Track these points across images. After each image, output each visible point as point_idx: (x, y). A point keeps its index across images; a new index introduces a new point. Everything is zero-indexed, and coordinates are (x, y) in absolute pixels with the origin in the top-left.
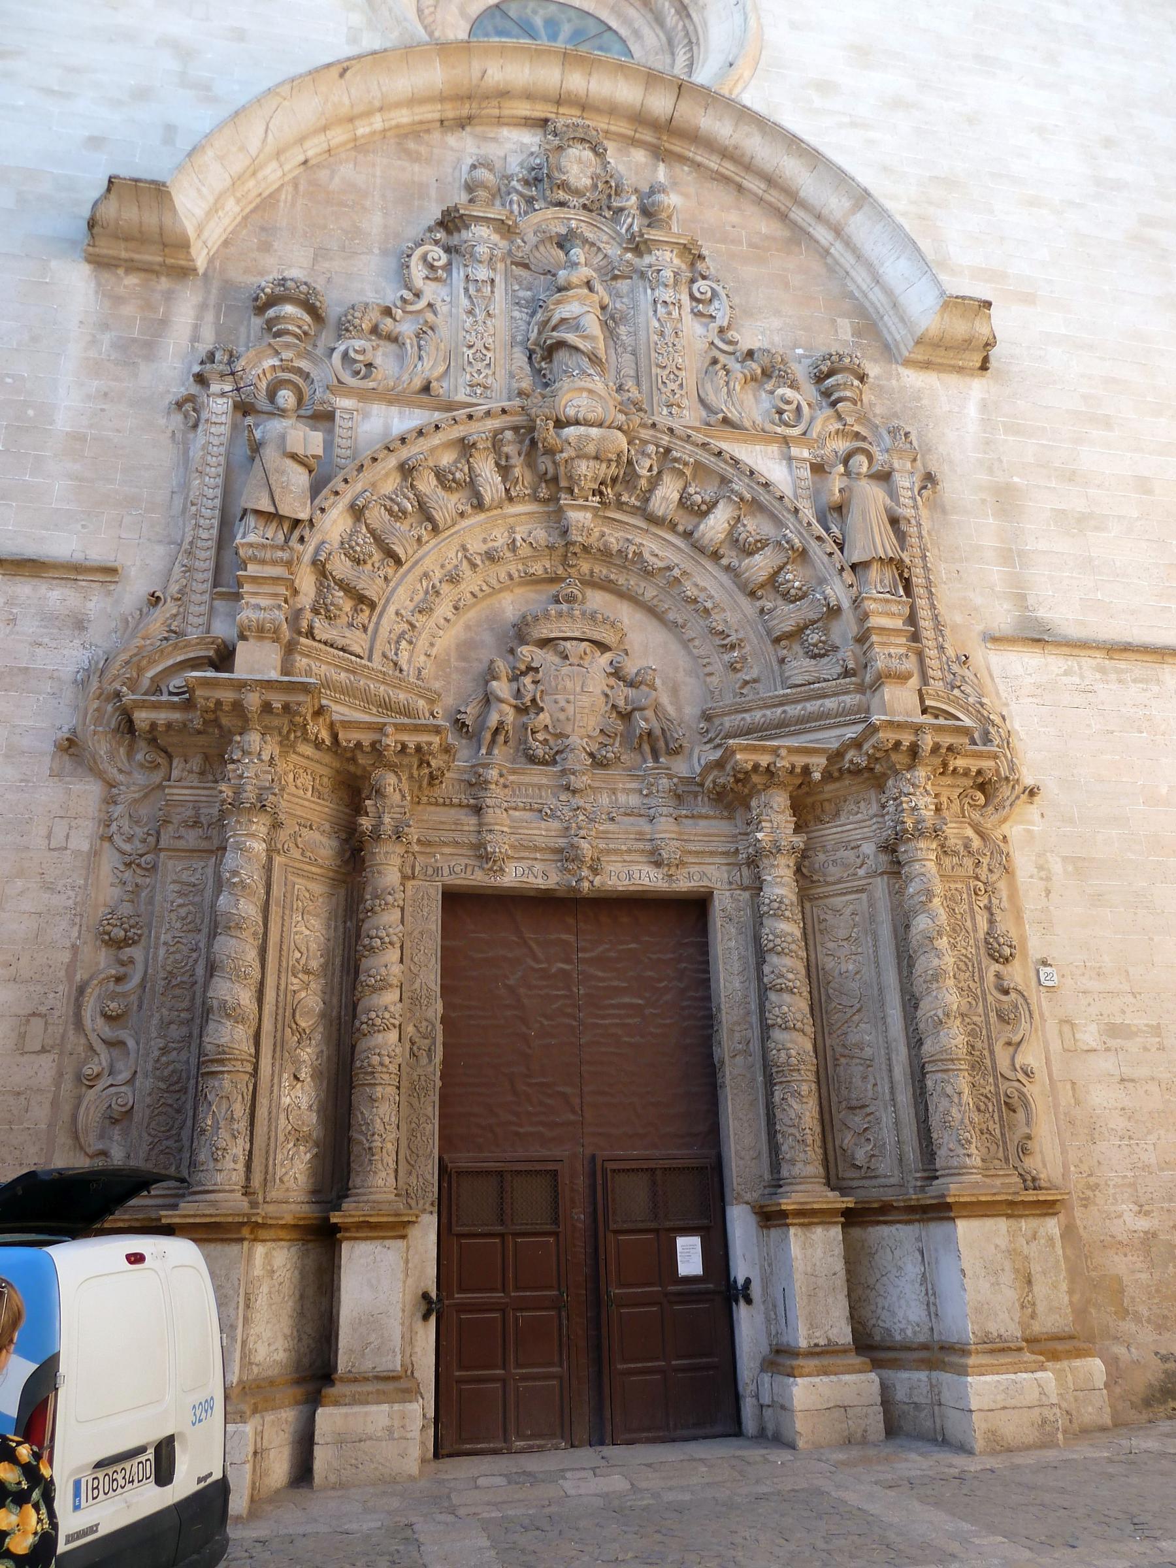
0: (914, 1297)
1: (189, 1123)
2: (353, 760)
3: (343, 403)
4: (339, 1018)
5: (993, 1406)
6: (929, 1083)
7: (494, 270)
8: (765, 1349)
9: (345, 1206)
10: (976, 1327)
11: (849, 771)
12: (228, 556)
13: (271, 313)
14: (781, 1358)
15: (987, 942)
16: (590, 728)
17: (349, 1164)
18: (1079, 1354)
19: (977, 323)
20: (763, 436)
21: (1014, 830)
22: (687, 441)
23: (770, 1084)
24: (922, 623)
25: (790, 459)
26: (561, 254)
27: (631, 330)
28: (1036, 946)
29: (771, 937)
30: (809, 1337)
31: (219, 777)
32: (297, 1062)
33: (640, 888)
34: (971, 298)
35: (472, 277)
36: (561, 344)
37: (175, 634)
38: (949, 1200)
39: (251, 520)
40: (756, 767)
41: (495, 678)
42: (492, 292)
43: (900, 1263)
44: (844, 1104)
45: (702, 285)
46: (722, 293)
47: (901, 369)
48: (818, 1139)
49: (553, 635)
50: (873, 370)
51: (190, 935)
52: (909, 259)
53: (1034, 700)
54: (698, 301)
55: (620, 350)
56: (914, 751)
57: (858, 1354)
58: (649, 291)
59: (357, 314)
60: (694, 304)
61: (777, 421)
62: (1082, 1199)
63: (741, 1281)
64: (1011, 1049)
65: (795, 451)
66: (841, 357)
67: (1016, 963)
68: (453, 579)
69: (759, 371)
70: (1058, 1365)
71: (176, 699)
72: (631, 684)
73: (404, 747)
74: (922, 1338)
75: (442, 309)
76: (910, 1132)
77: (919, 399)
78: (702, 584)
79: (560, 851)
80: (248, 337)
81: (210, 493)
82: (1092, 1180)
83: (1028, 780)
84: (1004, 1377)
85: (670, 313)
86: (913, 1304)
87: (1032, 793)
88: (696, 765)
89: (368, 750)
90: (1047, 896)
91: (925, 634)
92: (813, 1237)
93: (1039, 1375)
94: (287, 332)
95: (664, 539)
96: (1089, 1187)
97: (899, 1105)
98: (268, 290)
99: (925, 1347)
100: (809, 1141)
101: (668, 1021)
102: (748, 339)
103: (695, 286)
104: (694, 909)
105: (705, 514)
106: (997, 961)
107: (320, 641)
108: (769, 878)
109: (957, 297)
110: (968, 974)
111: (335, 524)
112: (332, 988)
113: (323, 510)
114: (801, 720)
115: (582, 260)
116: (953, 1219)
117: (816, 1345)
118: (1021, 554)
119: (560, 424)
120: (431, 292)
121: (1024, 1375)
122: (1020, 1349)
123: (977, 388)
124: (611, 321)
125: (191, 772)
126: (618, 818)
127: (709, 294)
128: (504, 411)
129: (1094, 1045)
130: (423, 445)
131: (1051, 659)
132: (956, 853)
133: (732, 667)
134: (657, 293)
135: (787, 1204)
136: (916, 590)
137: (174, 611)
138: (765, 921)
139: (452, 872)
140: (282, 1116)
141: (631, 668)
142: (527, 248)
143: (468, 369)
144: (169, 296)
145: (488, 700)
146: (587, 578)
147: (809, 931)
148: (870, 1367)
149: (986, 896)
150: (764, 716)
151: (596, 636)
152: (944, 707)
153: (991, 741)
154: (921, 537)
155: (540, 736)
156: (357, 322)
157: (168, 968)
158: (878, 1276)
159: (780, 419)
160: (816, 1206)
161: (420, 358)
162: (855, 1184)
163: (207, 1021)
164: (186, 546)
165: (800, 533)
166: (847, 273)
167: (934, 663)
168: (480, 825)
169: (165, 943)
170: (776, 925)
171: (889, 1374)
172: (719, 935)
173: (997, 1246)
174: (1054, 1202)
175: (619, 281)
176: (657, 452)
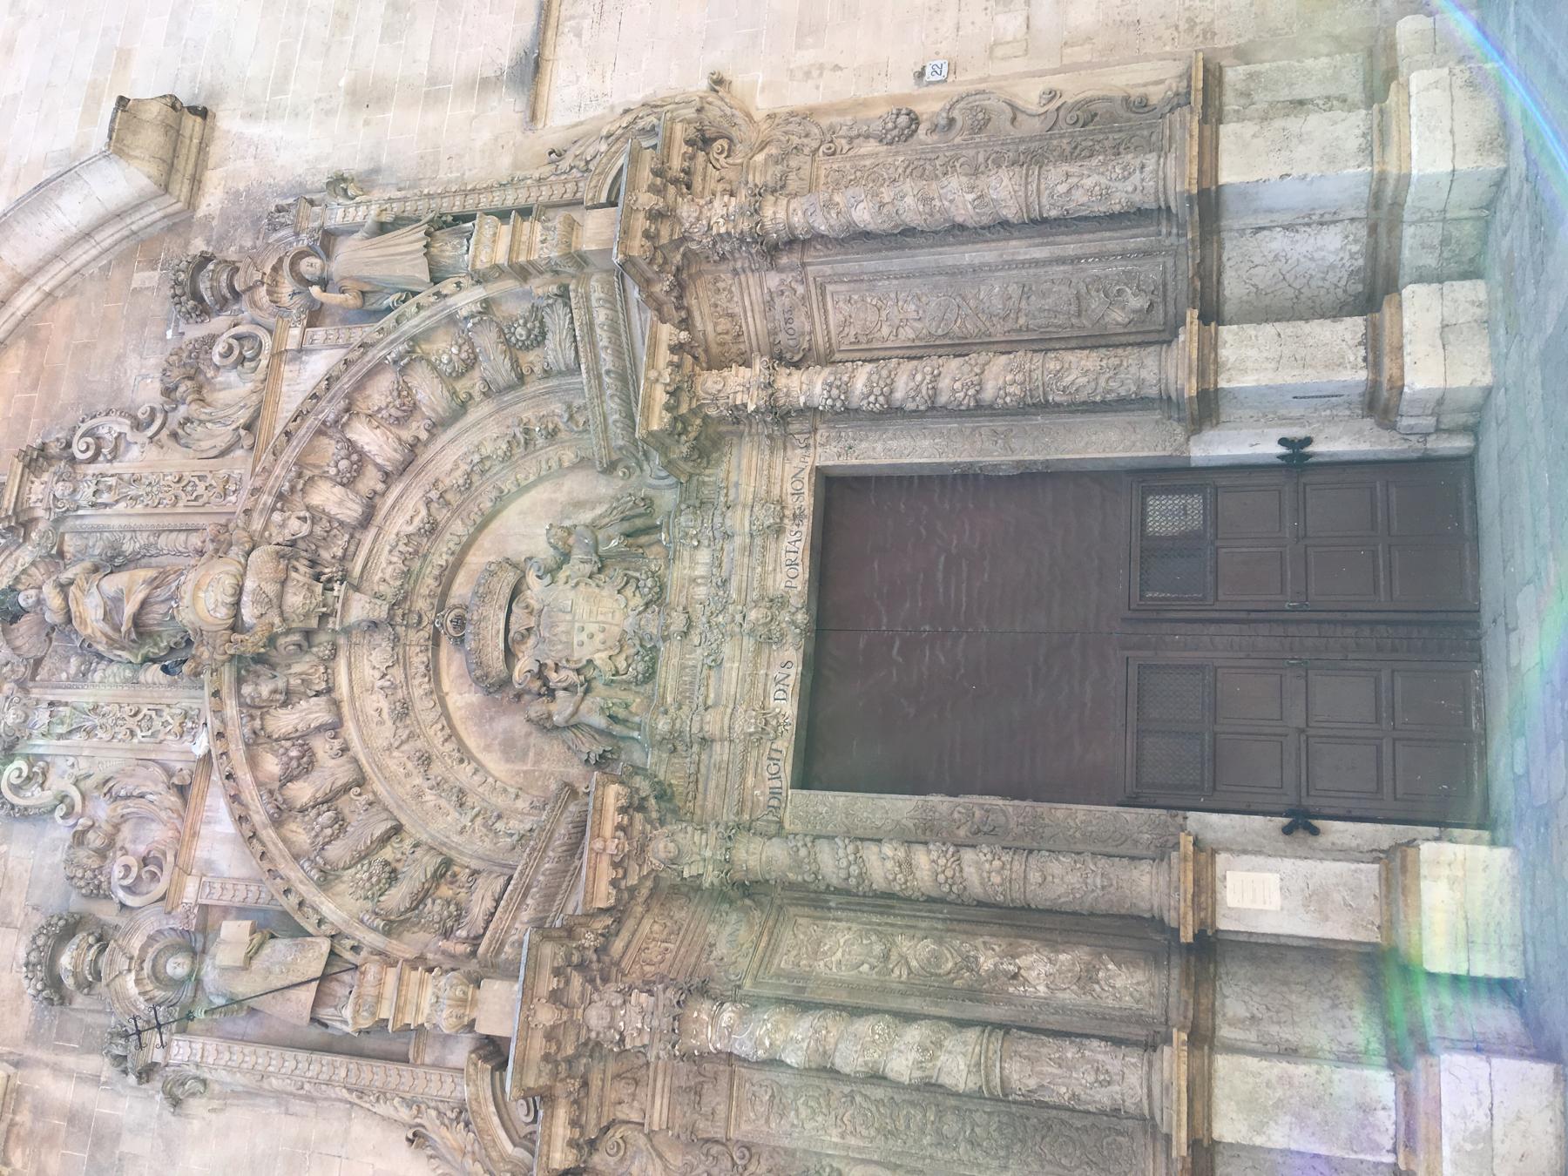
0: (1312, 240)
1: (1065, 1115)
2: (632, 890)
3: (190, 891)
4: (944, 920)
5: (1449, 145)
6: (1054, 213)
7: (38, 702)
8: (1369, 422)
9: (1174, 924)
10: (1352, 163)
11: (680, 297)
12: (370, 1043)
13: (69, 982)
14: (1379, 403)
15: (890, 143)
16: (615, 605)
17: (1122, 917)
18: (1391, 47)
19: (145, 116)
20: (271, 377)
21: (762, 105)
22: (270, 472)
23: (1045, 407)
24: (509, 203)
25: (300, 350)
26: (25, 619)
27: (128, 536)
28: (902, 85)
29: (872, 399)
30: (1354, 367)
31: (642, 1061)
32: (994, 975)
33: (808, 553)
34: (113, 121)
35: (44, 729)
36: (137, 621)
37: (463, 1114)
38: (1195, 191)
39: (325, 1013)
40: (668, 408)
41: (550, 716)
42: (66, 704)
43: (1271, 257)
44: (1074, 321)
45: (78, 448)
46: (89, 423)
47: (200, 213)
48: (1112, 352)
49: (502, 646)
50: (198, 246)
51: (834, 1103)
52: (60, 194)
53: (608, 75)
54: (98, 453)
55: (153, 552)
56: (655, 216)
57: (1379, 310)
58: (80, 512)
59: (79, 873)
60: (101, 458)
61: (253, 364)
62: (1205, 38)
63: (1282, 450)
64: (1020, 117)
65: (292, 345)
66: (177, 283)
67: (918, 109)
68: (426, 760)
69: (189, 383)
70: (1403, 69)
71: (541, 1113)
72: (566, 557)
73: (620, 827)
74: (1364, 233)
75: (84, 766)
76: (1112, 241)
77: (237, 194)
78: (449, 466)
79: (759, 645)
80: (99, 1012)
81: (290, 1064)
82: (1183, 26)
83: (704, 84)
84: (1413, 130)
85: (110, 488)
86: (1320, 243)
87: (718, 82)
88: (667, 482)
89: (621, 871)
90: (841, 69)
91: (522, 202)
92: (1232, 359)
93: (1413, 89)
94: (95, 961)
95: (393, 507)
96: (1191, 29)
97: (1079, 252)
98: (39, 986)
99: (1373, 230)
100: (1117, 361)
101: (967, 527)
102: (149, 394)
103: (80, 456)
104: (837, 492)
105: (362, 455)
106: (915, 131)
107: (486, 929)
108: (802, 400)
109: (110, 138)
110: (928, 167)
111: (336, 908)
112: (908, 927)
113: (320, 922)
114: (618, 353)
115: (33, 592)
116: (1219, 188)
117: (1365, 359)
118: (432, 80)
119: (236, 626)
120: (59, 782)
121: (1413, 107)
122: (1381, 111)
123: (228, 121)
124: (114, 562)
125: (634, 1095)
126: (724, 574)
127: (90, 440)
128: (216, 694)
129: (1021, 20)
130: (250, 794)
131: (560, 51)
132: (784, 177)
133: (552, 435)
134: (83, 503)
135: (1191, 389)
136: (469, 208)
137: (433, 1113)
138: (854, 405)
139: (776, 776)
140: (1060, 995)
141: (543, 551)
142: (15, 660)
143: (161, 737)
144: (39, 1111)
145: (573, 725)
146: (436, 602)
147: (868, 355)
148: (1395, 295)
149: (837, 141)
150: (612, 396)
151: (507, 592)
152: (609, 181)
153: (654, 127)
154: (405, 199)
155: (622, 665)
156: (89, 874)
157: (873, 1133)
158: (1284, 284)
159: (251, 360)
160: (1195, 356)
161: (142, 796)
162: (1171, 310)
163: (941, 1086)
164: (353, 1098)
165: (392, 342)
166: (76, 272)
167: (558, 191)
168: (722, 740)
169: (843, 1137)
170: (857, 392)
171: (1406, 272)
172: (868, 462)
173: (1254, 136)
174: (1206, 70)
175: (66, 548)
176: (282, 510)
